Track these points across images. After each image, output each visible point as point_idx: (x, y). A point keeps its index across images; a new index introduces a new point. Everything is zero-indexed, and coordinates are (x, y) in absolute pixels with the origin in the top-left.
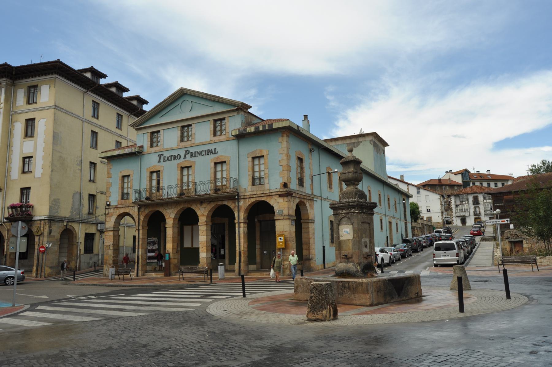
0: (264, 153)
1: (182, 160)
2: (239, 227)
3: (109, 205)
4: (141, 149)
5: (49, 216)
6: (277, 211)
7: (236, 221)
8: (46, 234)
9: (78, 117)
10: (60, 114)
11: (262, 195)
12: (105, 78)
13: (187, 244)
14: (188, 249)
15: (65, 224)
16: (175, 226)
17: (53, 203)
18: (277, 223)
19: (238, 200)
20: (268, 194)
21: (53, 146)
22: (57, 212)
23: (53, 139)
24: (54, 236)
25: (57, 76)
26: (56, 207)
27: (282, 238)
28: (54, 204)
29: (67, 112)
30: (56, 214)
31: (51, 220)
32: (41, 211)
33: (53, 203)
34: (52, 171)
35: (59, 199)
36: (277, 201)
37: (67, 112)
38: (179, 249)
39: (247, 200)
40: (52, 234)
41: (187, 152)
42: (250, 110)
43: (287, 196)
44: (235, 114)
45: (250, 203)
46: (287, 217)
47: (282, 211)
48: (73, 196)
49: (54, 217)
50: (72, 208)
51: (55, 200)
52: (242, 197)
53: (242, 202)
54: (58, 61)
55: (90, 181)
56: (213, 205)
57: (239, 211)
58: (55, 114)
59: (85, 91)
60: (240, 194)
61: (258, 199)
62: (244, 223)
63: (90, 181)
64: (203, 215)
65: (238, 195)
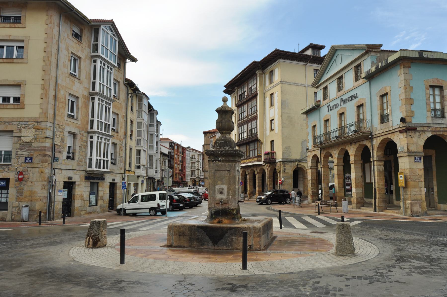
0: (388, 90)
1: (339, 107)
2: (374, 165)
3: (308, 149)
4: (318, 103)
5: (283, 159)
6: (399, 149)
7: (371, 160)
8: (282, 171)
9: (301, 85)
10: (286, 87)
11: (388, 133)
12: (324, 48)
13: (368, 181)
14: (368, 183)
15: (297, 163)
16: (339, 164)
17: (285, 149)
18: (400, 160)
19: (372, 139)
20: (392, 132)
21: (282, 110)
22: (289, 156)
23: (282, 105)
24: (288, 173)
25: (280, 60)
26: (288, 152)
27: (402, 176)
28: (286, 150)
29: (291, 84)
30: (288, 157)
31: (284, 162)
32: (279, 157)
33: (285, 149)
34: (282, 127)
35: (290, 147)
36: (399, 137)
37: (291, 84)
38: (363, 183)
39: (378, 138)
40: (286, 171)
41: (342, 100)
42: (382, 48)
43: (406, 132)
44: (366, 57)
45: (380, 141)
46: (406, 154)
47: (403, 148)
48: (302, 143)
49: (287, 159)
50: (301, 152)
51: (286, 148)
52: (375, 136)
53: (375, 141)
54: (277, 50)
55: (68, 157)
56: (357, 145)
57: (373, 150)
58: (281, 87)
59: (306, 64)
60: (374, 134)
61: (385, 137)
62: (379, 161)
63: (68, 157)
64: (353, 155)
65: (371, 134)
